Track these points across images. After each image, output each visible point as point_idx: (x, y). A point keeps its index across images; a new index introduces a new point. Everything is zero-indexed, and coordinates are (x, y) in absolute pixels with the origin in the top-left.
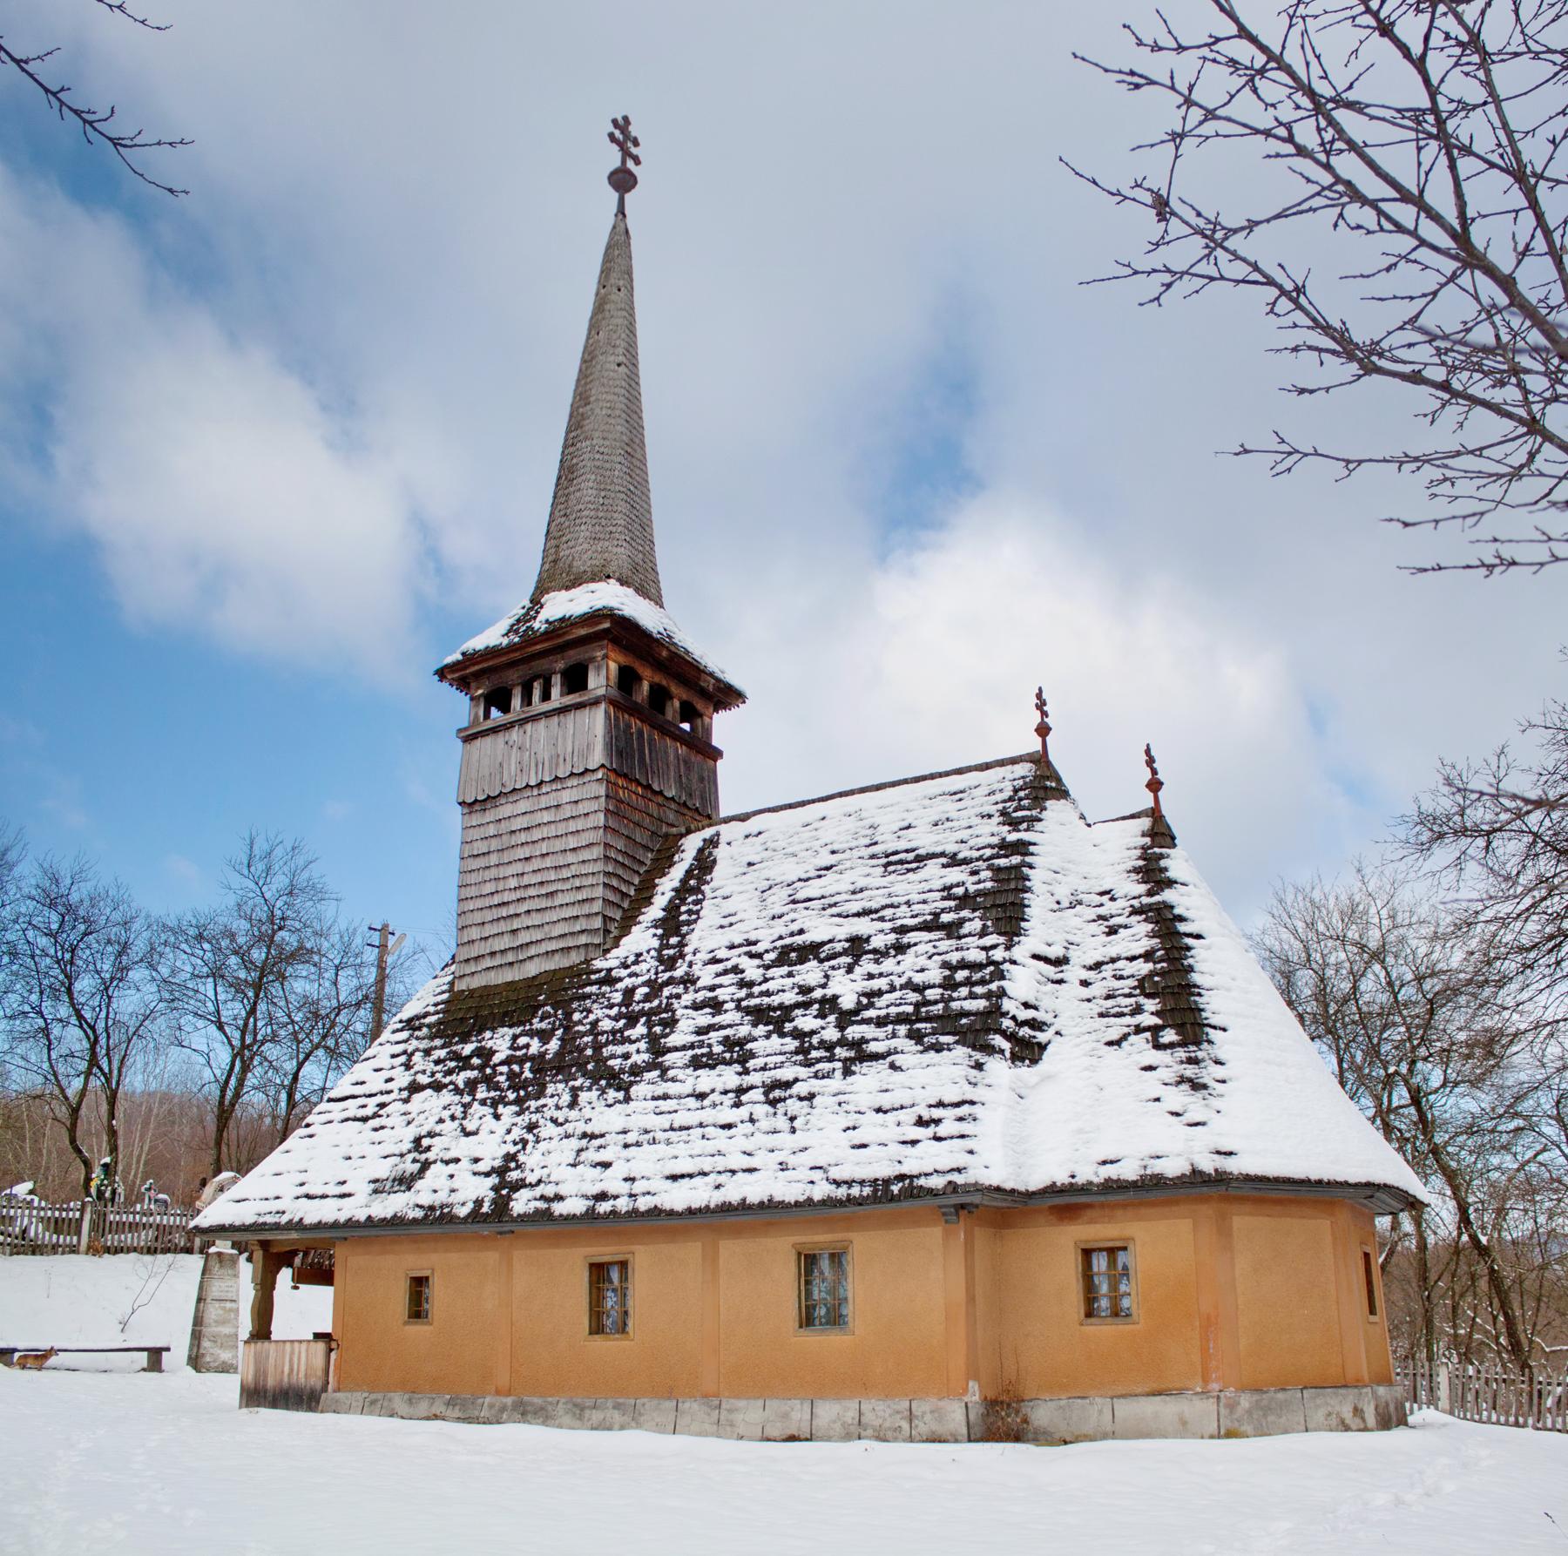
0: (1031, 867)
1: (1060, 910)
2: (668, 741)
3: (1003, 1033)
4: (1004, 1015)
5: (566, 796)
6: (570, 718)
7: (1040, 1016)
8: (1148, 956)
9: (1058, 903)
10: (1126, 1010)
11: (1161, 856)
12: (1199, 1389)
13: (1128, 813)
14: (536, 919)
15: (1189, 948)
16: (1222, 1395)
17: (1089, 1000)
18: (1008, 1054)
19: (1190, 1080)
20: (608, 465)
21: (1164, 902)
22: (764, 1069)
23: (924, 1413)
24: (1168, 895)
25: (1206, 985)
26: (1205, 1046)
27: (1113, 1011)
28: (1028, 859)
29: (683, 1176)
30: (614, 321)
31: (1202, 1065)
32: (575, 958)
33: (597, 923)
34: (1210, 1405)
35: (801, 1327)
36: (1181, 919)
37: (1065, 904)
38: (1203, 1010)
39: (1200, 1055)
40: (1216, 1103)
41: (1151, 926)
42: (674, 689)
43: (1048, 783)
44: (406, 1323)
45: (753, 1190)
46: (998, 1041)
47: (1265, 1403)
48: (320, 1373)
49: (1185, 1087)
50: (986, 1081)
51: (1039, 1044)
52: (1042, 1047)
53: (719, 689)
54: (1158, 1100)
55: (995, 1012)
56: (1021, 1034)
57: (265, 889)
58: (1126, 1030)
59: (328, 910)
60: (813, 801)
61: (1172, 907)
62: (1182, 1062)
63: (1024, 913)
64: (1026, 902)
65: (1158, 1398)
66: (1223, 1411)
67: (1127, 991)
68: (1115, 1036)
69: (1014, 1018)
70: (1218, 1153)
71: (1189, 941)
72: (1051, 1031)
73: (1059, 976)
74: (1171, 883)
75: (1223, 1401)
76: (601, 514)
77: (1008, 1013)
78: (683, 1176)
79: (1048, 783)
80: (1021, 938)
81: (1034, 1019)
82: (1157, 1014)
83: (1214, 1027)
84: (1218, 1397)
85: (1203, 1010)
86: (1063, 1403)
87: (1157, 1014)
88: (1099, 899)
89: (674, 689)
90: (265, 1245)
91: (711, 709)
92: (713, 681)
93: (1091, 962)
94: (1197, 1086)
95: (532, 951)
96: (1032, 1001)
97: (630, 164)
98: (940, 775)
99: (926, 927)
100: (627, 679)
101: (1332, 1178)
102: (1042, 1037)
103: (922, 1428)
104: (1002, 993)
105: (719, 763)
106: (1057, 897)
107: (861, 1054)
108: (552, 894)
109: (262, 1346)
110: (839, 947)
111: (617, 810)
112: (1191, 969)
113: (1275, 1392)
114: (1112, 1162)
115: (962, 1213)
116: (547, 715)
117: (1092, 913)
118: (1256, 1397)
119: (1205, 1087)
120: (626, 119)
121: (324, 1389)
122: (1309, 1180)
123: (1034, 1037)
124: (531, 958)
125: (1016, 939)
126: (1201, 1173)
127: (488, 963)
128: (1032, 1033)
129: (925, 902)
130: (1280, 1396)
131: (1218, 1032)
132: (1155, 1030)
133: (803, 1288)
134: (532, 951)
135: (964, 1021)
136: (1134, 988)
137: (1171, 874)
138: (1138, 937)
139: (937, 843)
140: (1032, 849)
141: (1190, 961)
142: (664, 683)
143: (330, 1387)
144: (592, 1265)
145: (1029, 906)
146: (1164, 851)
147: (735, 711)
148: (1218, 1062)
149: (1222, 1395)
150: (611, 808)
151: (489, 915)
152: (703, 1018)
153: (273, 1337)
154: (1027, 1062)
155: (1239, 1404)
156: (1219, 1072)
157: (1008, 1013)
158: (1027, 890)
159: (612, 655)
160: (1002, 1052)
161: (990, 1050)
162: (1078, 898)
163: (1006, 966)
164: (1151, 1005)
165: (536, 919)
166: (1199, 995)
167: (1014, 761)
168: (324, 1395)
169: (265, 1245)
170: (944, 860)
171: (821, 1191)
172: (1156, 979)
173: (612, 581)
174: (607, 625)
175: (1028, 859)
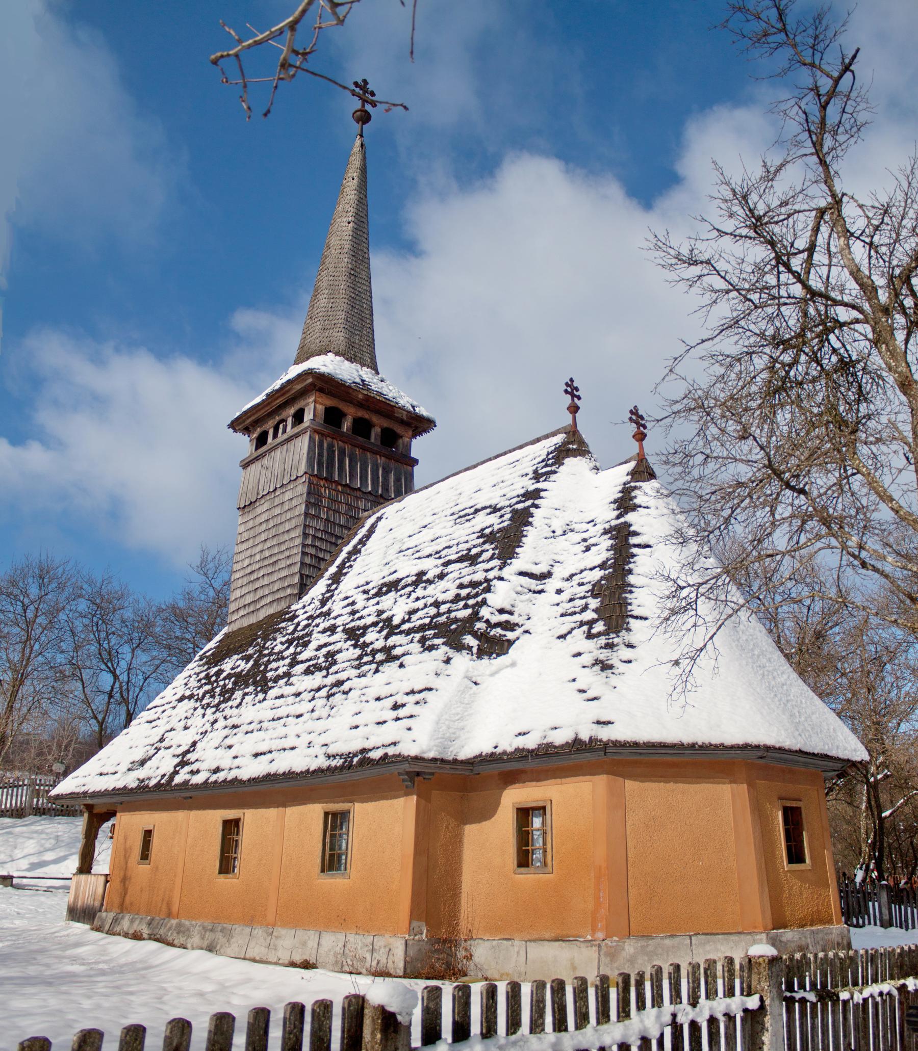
0: (537, 507)
1: (554, 537)
2: (369, 454)
3: (475, 635)
4: (480, 619)
5: (287, 496)
6: (291, 445)
7: (513, 619)
8: (602, 566)
9: (554, 532)
10: (577, 610)
11: (635, 488)
12: (589, 937)
13: (623, 461)
14: (266, 581)
15: (633, 556)
16: (603, 944)
17: (558, 605)
18: (475, 650)
19: (602, 662)
20: (337, 283)
21: (626, 522)
22: (336, 673)
23: (380, 947)
24: (630, 517)
25: (638, 584)
26: (623, 633)
27: (569, 611)
28: (536, 502)
29: (261, 754)
30: (348, 197)
31: (615, 649)
32: (283, 605)
33: (296, 579)
34: (592, 952)
35: (323, 871)
36: (636, 534)
37: (559, 532)
38: (630, 604)
39: (616, 641)
40: (614, 680)
41: (611, 542)
42: (375, 419)
43: (571, 446)
44: (139, 864)
45: (283, 763)
46: (469, 640)
47: (650, 948)
48: (100, 898)
49: (597, 668)
50: (447, 672)
51: (508, 641)
52: (511, 643)
53: (412, 418)
54: (574, 680)
55: (475, 617)
56: (492, 633)
57: (213, 581)
58: (573, 625)
59: (196, 589)
60: (436, 483)
61: (630, 525)
62: (601, 648)
63: (521, 541)
64: (525, 533)
65: (557, 943)
66: (603, 958)
67: (582, 595)
68: (563, 631)
69: (487, 621)
70: (598, 723)
71: (635, 550)
72: (519, 631)
73: (540, 588)
74: (635, 508)
75: (604, 949)
76: (330, 313)
77: (483, 617)
78: (261, 754)
79: (571, 446)
80: (513, 560)
81: (507, 622)
82: (595, 611)
83: (636, 618)
84: (599, 946)
85: (630, 604)
86: (495, 943)
87: (595, 611)
88: (585, 526)
89: (375, 419)
90: (89, 808)
91: (410, 433)
92: (405, 413)
93: (567, 575)
94: (605, 666)
95: (263, 602)
96: (508, 608)
97: (368, 107)
98: (510, 451)
99: (460, 560)
100: (332, 417)
101: (707, 742)
102: (510, 635)
103: (347, 969)
104: (484, 602)
105: (416, 468)
106: (552, 529)
107: (390, 655)
108: (275, 562)
109: (83, 877)
110: (409, 580)
111: (313, 499)
112: (630, 572)
113: (662, 938)
114: (525, 734)
115: (417, 779)
116: (282, 444)
117: (578, 537)
118: (642, 943)
119: (611, 667)
120: (365, 82)
121: (100, 911)
122: (683, 745)
123: (505, 636)
124: (262, 607)
125: (509, 561)
126: (581, 740)
127: (242, 613)
128: (503, 633)
129: (467, 542)
130: (668, 942)
131: (639, 621)
132: (591, 623)
133: (328, 840)
134: (263, 602)
135: (454, 626)
136: (587, 592)
137: (636, 501)
138: (602, 551)
139: (491, 498)
140: (542, 494)
141: (631, 566)
142: (367, 416)
143: (104, 908)
144: (518, 809)
145: (526, 536)
146: (638, 484)
147: (432, 432)
148: (630, 646)
149: (603, 944)
150: (312, 501)
151: (245, 581)
152: (324, 639)
153: (93, 871)
154: (494, 655)
155: (623, 949)
156: (626, 653)
157: (483, 617)
158: (530, 524)
159: (320, 400)
160: (470, 648)
161: (459, 647)
162: (572, 527)
163: (495, 582)
164: (594, 603)
165: (266, 581)
166: (631, 592)
167: (554, 434)
168: (99, 914)
169: (89, 808)
170: (489, 510)
171: (323, 762)
172: (603, 582)
173: (330, 354)
174: (310, 380)
175: (536, 502)
